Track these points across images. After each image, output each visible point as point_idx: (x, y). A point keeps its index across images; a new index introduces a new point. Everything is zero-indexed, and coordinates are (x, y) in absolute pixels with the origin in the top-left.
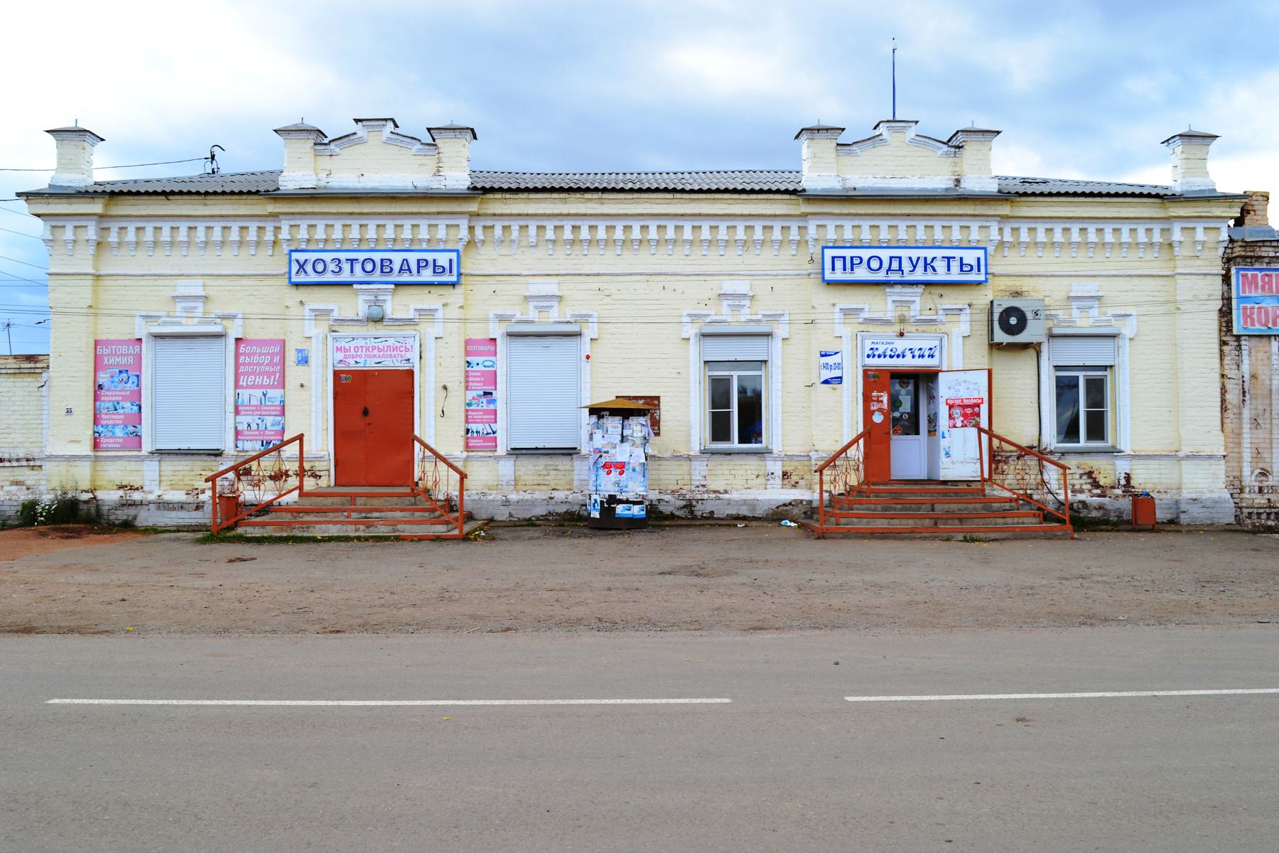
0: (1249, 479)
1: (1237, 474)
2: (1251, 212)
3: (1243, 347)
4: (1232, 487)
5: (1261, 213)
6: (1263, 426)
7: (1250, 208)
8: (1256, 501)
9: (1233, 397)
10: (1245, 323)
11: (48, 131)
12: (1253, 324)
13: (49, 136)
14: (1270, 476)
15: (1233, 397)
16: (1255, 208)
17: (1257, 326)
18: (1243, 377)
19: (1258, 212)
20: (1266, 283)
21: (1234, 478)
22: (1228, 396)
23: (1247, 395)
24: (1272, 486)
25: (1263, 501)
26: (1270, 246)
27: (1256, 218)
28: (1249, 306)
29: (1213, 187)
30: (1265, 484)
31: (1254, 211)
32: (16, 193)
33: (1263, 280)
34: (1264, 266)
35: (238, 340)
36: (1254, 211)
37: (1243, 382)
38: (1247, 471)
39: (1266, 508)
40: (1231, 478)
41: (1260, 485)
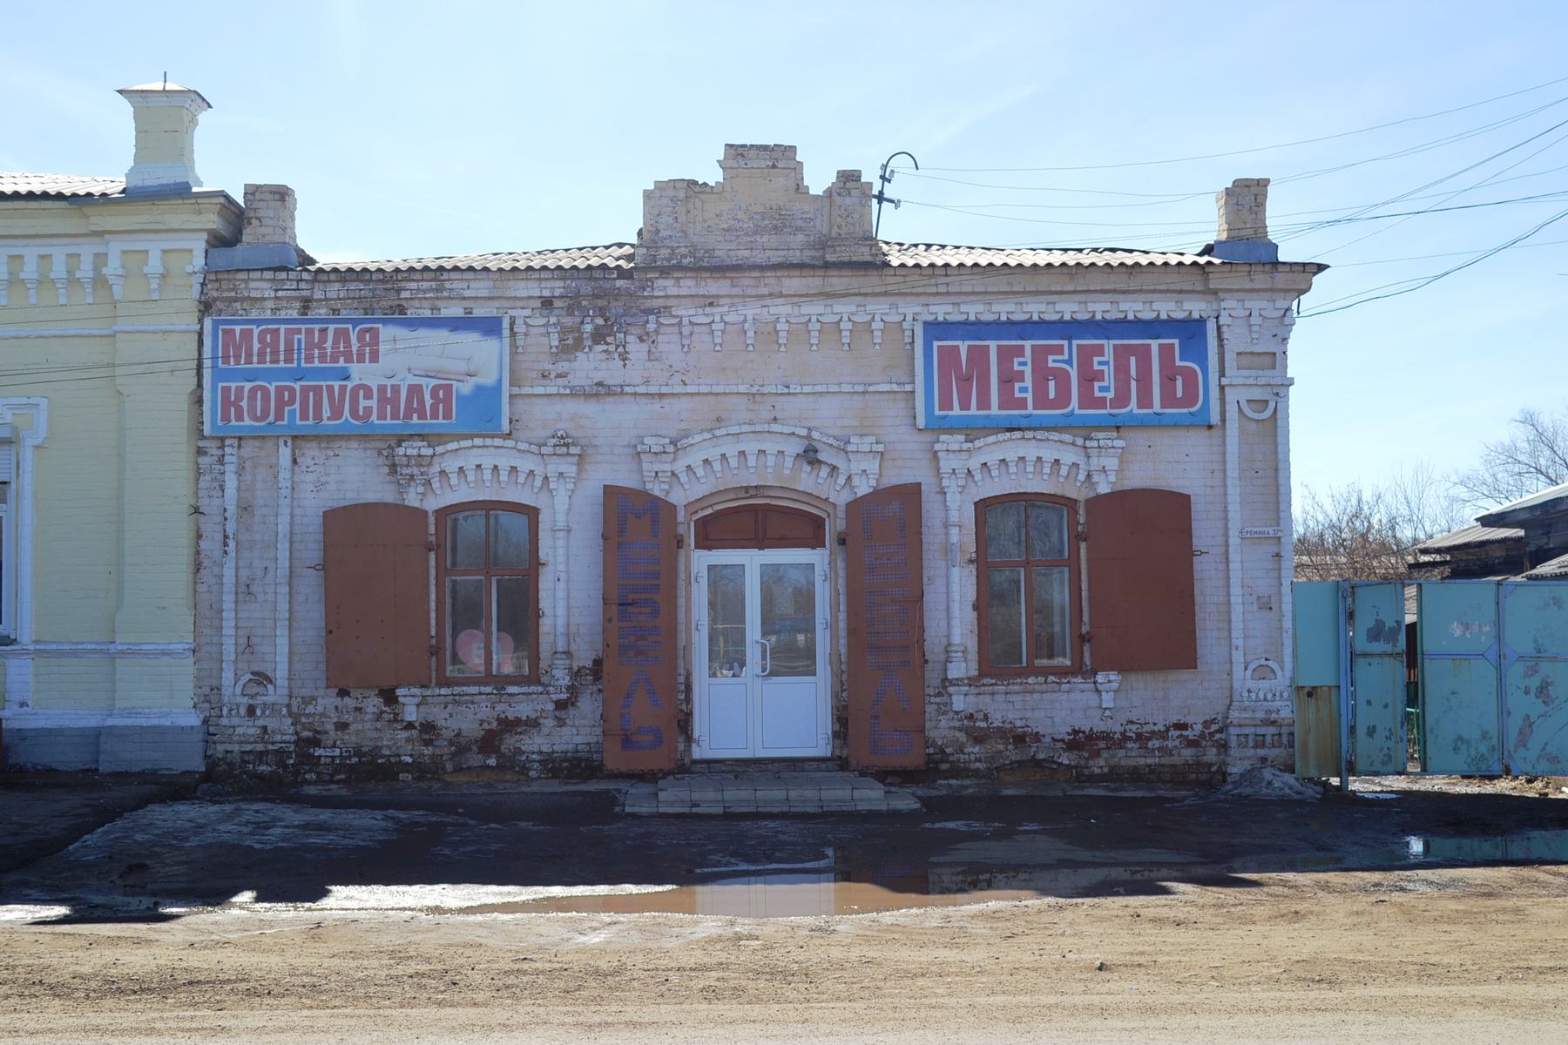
0: (231, 686)
1: (214, 683)
2: (253, 221)
3: (227, 459)
4: (207, 705)
5: (270, 222)
6: (260, 597)
7: (252, 214)
8: (240, 731)
9: (210, 545)
10: (226, 418)
11: (120, 92)
12: (240, 417)
13: (124, 103)
14: (269, 686)
15: (210, 545)
16: (261, 214)
17: (247, 422)
18: (225, 510)
19: (265, 222)
20: (267, 345)
21: (212, 689)
22: (203, 545)
23: (232, 544)
24: (273, 704)
25: (251, 731)
26: (262, 279)
27: (262, 230)
28: (233, 385)
29: (185, 180)
30: (259, 700)
31: (258, 218)
32: (1263, 184)
33: (262, 340)
34: (268, 315)
35: (1191, 331)
36: (258, 218)
37: (226, 519)
38: (228, 676)
39: (256, 742)
40: (206, 690)
41: (251, 702)
